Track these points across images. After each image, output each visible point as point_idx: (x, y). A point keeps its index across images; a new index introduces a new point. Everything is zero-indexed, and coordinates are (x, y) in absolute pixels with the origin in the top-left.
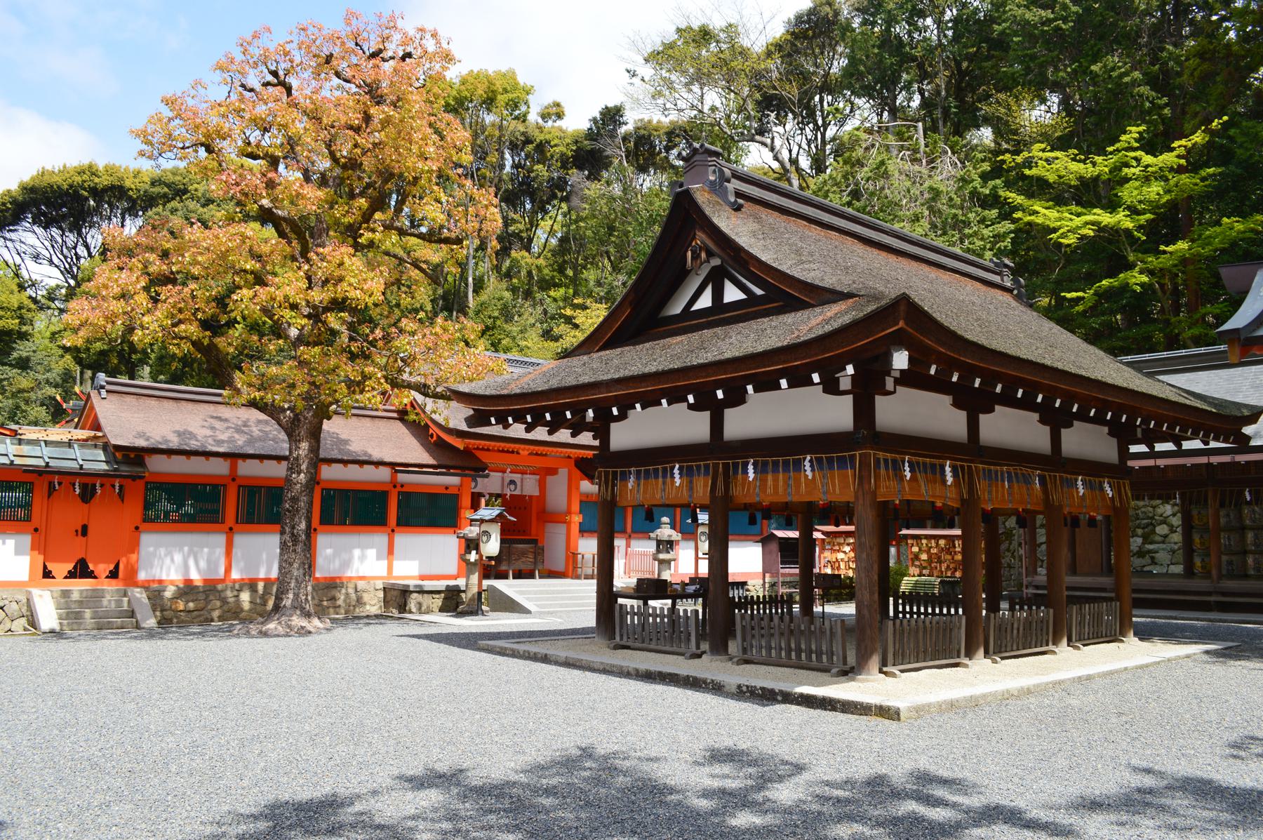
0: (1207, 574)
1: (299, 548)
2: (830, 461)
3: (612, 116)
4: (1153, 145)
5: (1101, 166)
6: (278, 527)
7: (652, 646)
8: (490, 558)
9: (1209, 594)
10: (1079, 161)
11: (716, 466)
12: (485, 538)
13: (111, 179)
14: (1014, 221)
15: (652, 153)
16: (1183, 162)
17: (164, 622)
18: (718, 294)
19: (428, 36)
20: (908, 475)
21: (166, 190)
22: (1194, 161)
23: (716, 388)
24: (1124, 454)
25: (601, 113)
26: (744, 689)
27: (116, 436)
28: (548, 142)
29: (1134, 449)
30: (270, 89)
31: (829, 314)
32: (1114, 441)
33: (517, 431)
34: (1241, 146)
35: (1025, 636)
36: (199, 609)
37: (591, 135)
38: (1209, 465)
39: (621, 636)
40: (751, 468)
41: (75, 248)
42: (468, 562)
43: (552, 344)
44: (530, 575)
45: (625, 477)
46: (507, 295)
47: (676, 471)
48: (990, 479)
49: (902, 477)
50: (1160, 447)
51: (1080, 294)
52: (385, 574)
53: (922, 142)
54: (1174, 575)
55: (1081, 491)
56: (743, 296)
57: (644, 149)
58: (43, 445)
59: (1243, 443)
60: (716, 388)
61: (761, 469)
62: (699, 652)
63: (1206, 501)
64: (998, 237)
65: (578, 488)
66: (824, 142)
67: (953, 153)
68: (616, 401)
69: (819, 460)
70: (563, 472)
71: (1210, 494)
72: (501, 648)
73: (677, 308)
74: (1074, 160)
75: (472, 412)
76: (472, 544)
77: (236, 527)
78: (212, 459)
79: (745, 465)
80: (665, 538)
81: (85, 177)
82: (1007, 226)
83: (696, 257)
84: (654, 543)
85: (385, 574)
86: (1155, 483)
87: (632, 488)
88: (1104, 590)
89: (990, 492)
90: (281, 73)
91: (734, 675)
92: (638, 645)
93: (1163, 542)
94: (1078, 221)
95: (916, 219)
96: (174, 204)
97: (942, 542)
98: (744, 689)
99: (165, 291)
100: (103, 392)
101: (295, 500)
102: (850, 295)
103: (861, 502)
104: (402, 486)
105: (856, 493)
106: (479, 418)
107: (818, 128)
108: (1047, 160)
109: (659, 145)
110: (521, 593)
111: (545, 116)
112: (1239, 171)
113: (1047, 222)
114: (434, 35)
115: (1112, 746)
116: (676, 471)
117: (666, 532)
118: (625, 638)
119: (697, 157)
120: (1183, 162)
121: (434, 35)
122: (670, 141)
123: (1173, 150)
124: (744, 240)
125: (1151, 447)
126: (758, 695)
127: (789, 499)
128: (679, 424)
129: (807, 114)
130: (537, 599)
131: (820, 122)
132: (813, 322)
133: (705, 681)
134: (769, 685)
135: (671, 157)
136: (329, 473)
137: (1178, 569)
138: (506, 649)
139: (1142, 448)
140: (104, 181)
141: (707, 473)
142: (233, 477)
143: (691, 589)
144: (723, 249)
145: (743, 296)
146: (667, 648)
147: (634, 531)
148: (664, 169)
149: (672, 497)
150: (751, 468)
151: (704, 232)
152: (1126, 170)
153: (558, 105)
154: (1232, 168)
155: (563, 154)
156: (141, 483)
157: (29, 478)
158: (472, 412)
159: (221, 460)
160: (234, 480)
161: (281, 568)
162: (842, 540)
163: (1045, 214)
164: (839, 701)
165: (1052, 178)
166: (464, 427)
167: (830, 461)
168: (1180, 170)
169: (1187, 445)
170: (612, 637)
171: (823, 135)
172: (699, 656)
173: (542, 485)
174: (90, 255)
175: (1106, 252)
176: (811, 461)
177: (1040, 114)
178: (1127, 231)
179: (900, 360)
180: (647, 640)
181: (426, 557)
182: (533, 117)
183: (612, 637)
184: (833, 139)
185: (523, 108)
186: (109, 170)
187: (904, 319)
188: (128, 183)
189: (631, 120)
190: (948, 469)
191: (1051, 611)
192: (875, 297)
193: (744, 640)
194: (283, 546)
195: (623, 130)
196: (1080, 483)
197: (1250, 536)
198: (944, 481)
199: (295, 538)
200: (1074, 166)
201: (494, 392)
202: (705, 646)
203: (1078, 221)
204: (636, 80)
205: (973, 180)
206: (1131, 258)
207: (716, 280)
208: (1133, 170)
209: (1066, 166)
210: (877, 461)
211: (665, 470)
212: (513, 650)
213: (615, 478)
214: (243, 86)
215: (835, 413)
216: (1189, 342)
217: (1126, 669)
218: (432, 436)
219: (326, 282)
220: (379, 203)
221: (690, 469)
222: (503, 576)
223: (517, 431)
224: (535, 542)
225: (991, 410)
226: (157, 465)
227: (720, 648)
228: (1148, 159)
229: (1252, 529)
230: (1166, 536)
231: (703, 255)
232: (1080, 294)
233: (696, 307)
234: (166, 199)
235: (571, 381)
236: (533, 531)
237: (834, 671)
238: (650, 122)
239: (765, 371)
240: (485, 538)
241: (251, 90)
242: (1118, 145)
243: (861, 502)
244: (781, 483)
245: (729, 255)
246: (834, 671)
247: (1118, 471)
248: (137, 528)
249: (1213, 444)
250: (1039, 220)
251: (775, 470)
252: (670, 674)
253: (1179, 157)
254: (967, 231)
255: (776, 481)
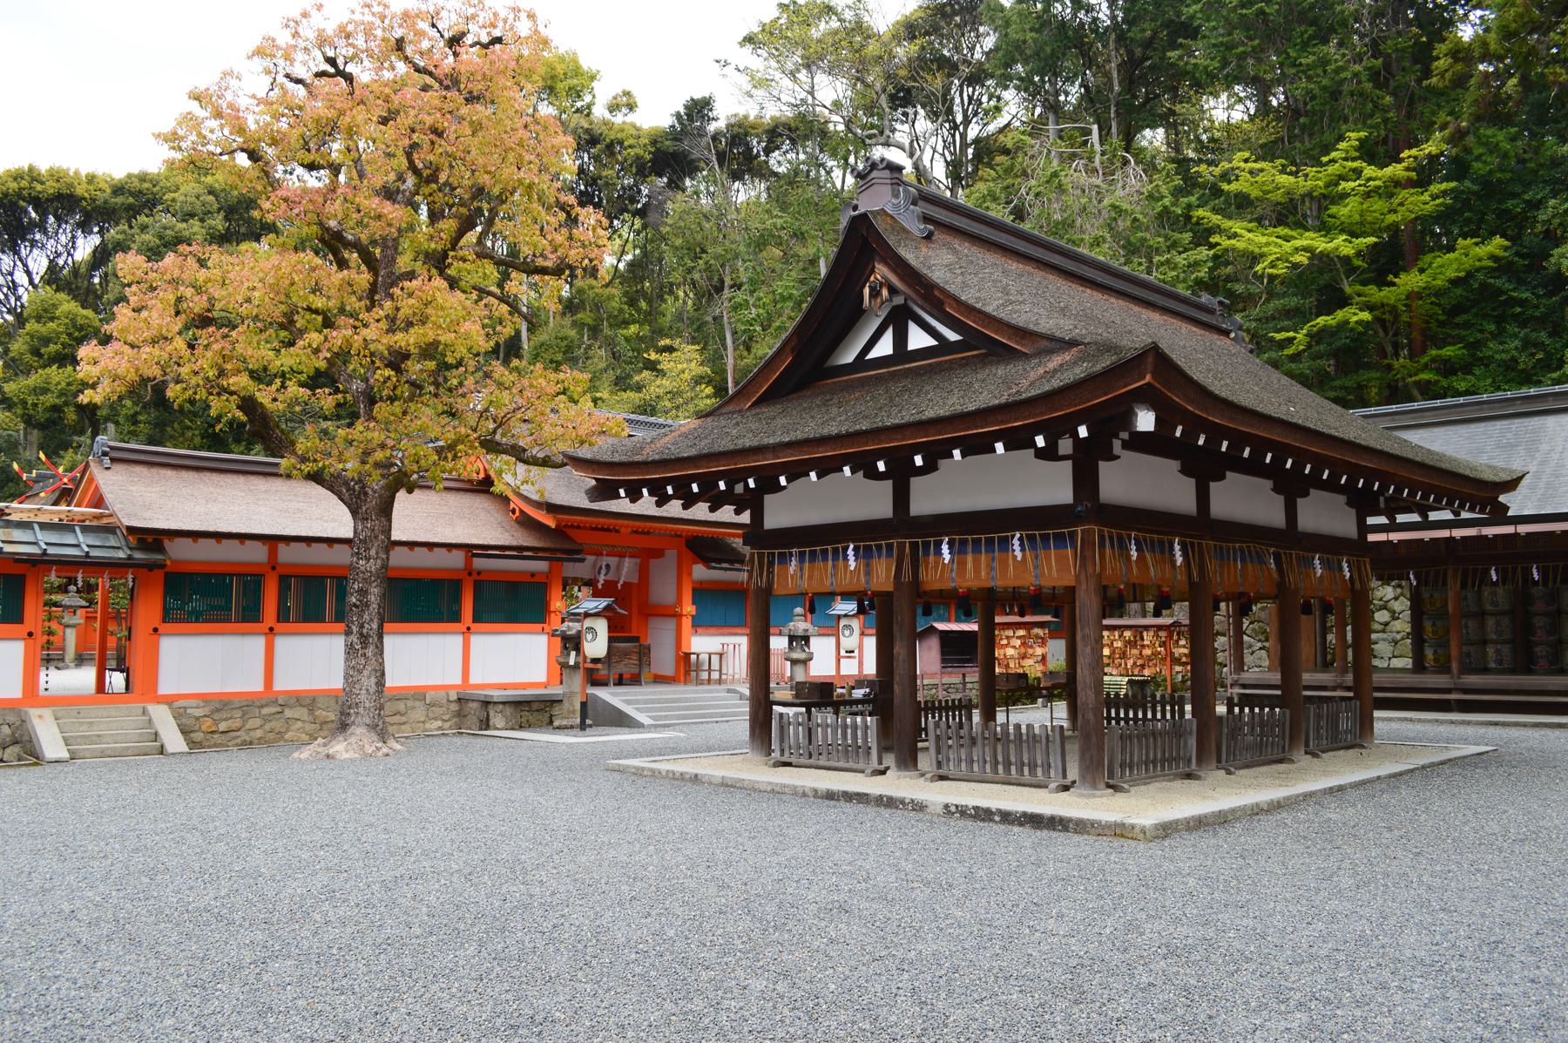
0: (1444, 669)
1: (370, 652)
2: (1045, 538)
3: (699, 109)
4: (1372, 152)
5: (1312, 179)
6: (341, 626)
7: (821, 763)
8: (595, 661)
9: (1449, 691)
10: (1290, 174)
11: (901, 547)
12: (589, 637)
13: (57, 185)
14: (1212, 246)
15: (749, 157)
16: (1413, 175)
17: (192, 744)
18: (901, 339)
19: (523, 16)
20: (1134, 554)
21: (131, 200)
22: (1423, 176)
23: (898, 457)
24: (1364, 529)
25: (686, 107)
26: (953, 809)
27: (129, 515)
28: (621, 143)
29: (1371, 521)
30: (324, 80)
31: (1051, 365)
32: (1353, 511)
33: (646, 505)
34: (1478, 158)
35: (1291, 738)
36: (217, 725)
37: (674, 135)
38: (1451, 539)
39: (782, 751)
40: (945, 548)
41: (11, 274)
42: (564, 666)
43: (631, 395)
44: (635, 680)
45: (784, 559)
46: (573, 333)
47: (850, 552)
48: (1222, 558)
49: (1129, 557)
50: (1401, 518)
51: (1291, 334)
52: (458, 681)
53: (1097, 147)
54: (1395, 670)
55: (1319, 572)
56: (932, 342)
57: (740, 152)
58: (30, 526)
59: (1500, 514)
60: (898, 457)
61: (958, 549)
62: (882, 767)
63: (1444, 583)
64: (1195, 265)
65: (690, 574)
66: (964, 145)
67: (1137, 163)
68: (784, 468)
69: (1031, 538)
70: (671, 555)
71: (1450, 573)
72: (637, 768)
73: (849, 357)
74: (1283, 172)
75: (594, 482)
76: (573, 642)
77: (279, 627)
78: (224, 541)
79: (938, 545)
80: (800, 633)
81: (24, 183)
82: (1204, 253)
83: (875, 293)
84: (786, 639)
85: (458, 681)
86: (1390, 563)
87: (794, 573)
88: (1324, 688)
89: (1222, 576)
90: (340, 61)
91: (938, 795)
92: (803, 761)
93: (1383, 631)
94: (1288, 247)
95: (1097, 242)
96: (142, 219)
97: (1127, 634)
98: (953, 809)
99: (204, 335)
100: (107, 460)
101: (363, 592)
102: (1072, 343)
103: (1084, 587)
104: (479, 573)
105: (1077, 577)
106: (605, 490)
107: (956, 127)
108: (1251, 172)
109: (757, 146)
110: (628, 702)
111: (613, 108)
112: (1475, 188)
113: (1251, 248)
114: (532, 16)
115: (1395, 862)
116: (850, 552)
117: (800, 626)
118: (787, 753)
119: (875, 174)
120: (1413, 175)
121: (532, 16)
122: (770, 141)
123: (1400, 161)
124: (938, 275)
125: (1392, 519)
126: (971, 816)
127: (993, 584)
128: (857, 497)
129: (940, 109)
130: (649, 710)
131: (959, 119)
132: (1033, 375)
133: (902, 802)
134: (984, 803)
135: (772, 162)
136: (399, 558)
137: (1407, 662)
138: (643, 769)
139: (1383, 520)
140: (51, 188)
141: (890, 554)
142: (469, 571)
143: (858, 693)
144: (909, 285)
145: (932, 342)
146: (841, 764)
147: (283, 616)
148: (762, 177)
149: (846, 583)
150: (945, 548)
151: (886, 264)
152: (1343, 184)
153: (627, 94)
154: (1467, 183)
155: (638, 158)
156: (159, 575)
157: (16, 570)
158: (594, 482)
159: (258, 544)
160: (274, 568)
161: (347, 676)
162: (1010, 633)
163: (1245, 236)
164: (1070, 820)
165: (1255, 193)
166: (585, 503)
167: (1045, 538)
168: (1410, 183)
169: (1434, 516)
170: (769, 752)
171: (963, 136)
172: (883, 773)
173: (644, 572)
174: (31, 282)
175: (1322, 284)
176: (1021, 539)
177: (1226, 110)
178: (1346, 260)
179: (1145, 421)
180: (815, 756)
181: (515, 658)
182: (599, 112)
183: (769, 752)
184: (977, 141)
185: (588, 98)
186: (57, 175)
187: (1155, 373)
188: (80, 191)
189: (723, 116)
190: (1177, 547)
191: (1288, 712)
192: (1109, 348)
193: (938, 752)
194: (350, 650)
195: (712, 128)
196: (1317, 562)
197: (1491, 622)
198: (1173, 562)
199: (364, 639)
200: (1285, 180)
201: (624, 458)
202: (890, 760)
203: (1288, 247)
204: (729, 70)
205: (1163, 197)
206: (1348, 290)
207: (899, 320)
208: (1352, 184)
209: (1276, 179)
210: (1102, 538)
211: (836, 551)
212: (652, 770)
213: (771, 564)
214: (287, 76)
215: (1051, 486)
216: (1415, 392)
217: (1379, 778)
218: (513, 511)
219: (410, 324)
220: (467, 225)
221: (868, 549)
222: (603, 683)
223: (646, 505)
224: (636, 639)
225: (1222, 477)
226: (179, 551)
227: (908, 760)
228: (1370, 171)
229: (1493, 614)
230: (1386, 624)
231: (885, 292)
232: (1291, 334)
233: (874, 354)
234: (132, 212)
235: (725, 445)
236: (634, 626)
237: (1053, 785)
238: (746, 117)
239: (972, 435)
240: (589, 637)
241: (298, 81)
242: (1334, 154)
243: (1084, 587)
244: (983, 565)
245: (918, 293)
246: (1053, 785)
247: (1356, 547)
248: (155, 630)
249: (1465, 515)
250: (1240, 245)
251: (976, 550)
252: (858, 794)
253: (1407, 169)
254: (1156, 259)
255: (976, 563)
